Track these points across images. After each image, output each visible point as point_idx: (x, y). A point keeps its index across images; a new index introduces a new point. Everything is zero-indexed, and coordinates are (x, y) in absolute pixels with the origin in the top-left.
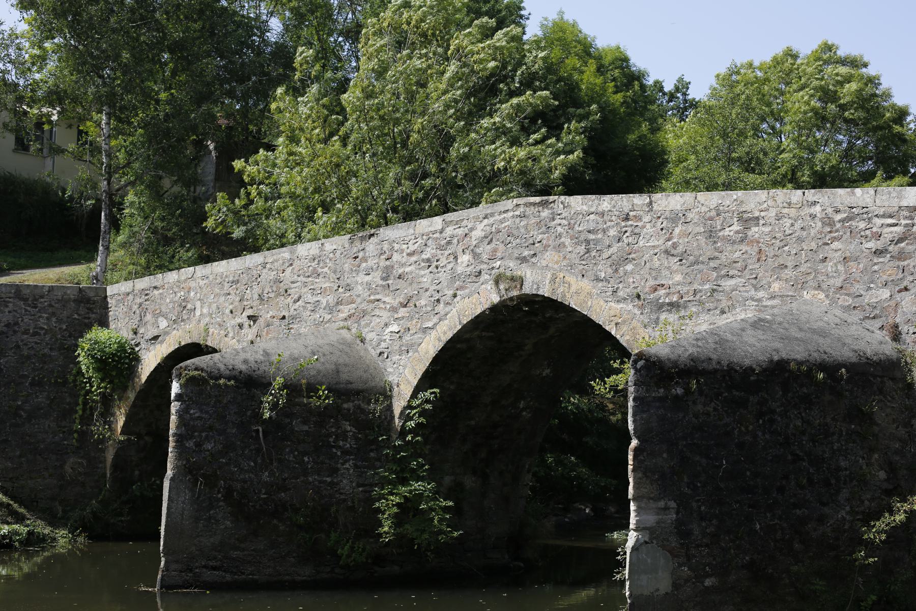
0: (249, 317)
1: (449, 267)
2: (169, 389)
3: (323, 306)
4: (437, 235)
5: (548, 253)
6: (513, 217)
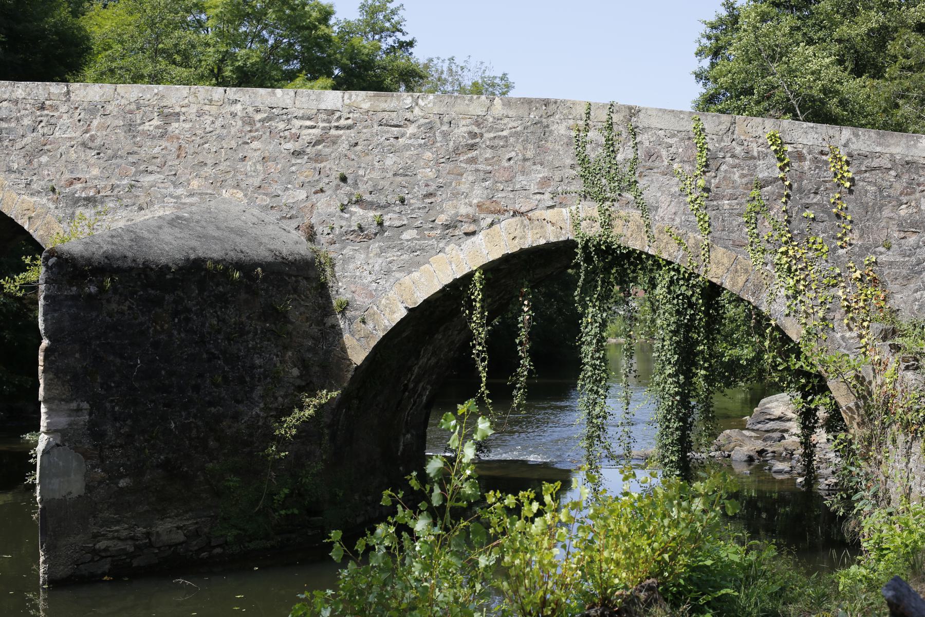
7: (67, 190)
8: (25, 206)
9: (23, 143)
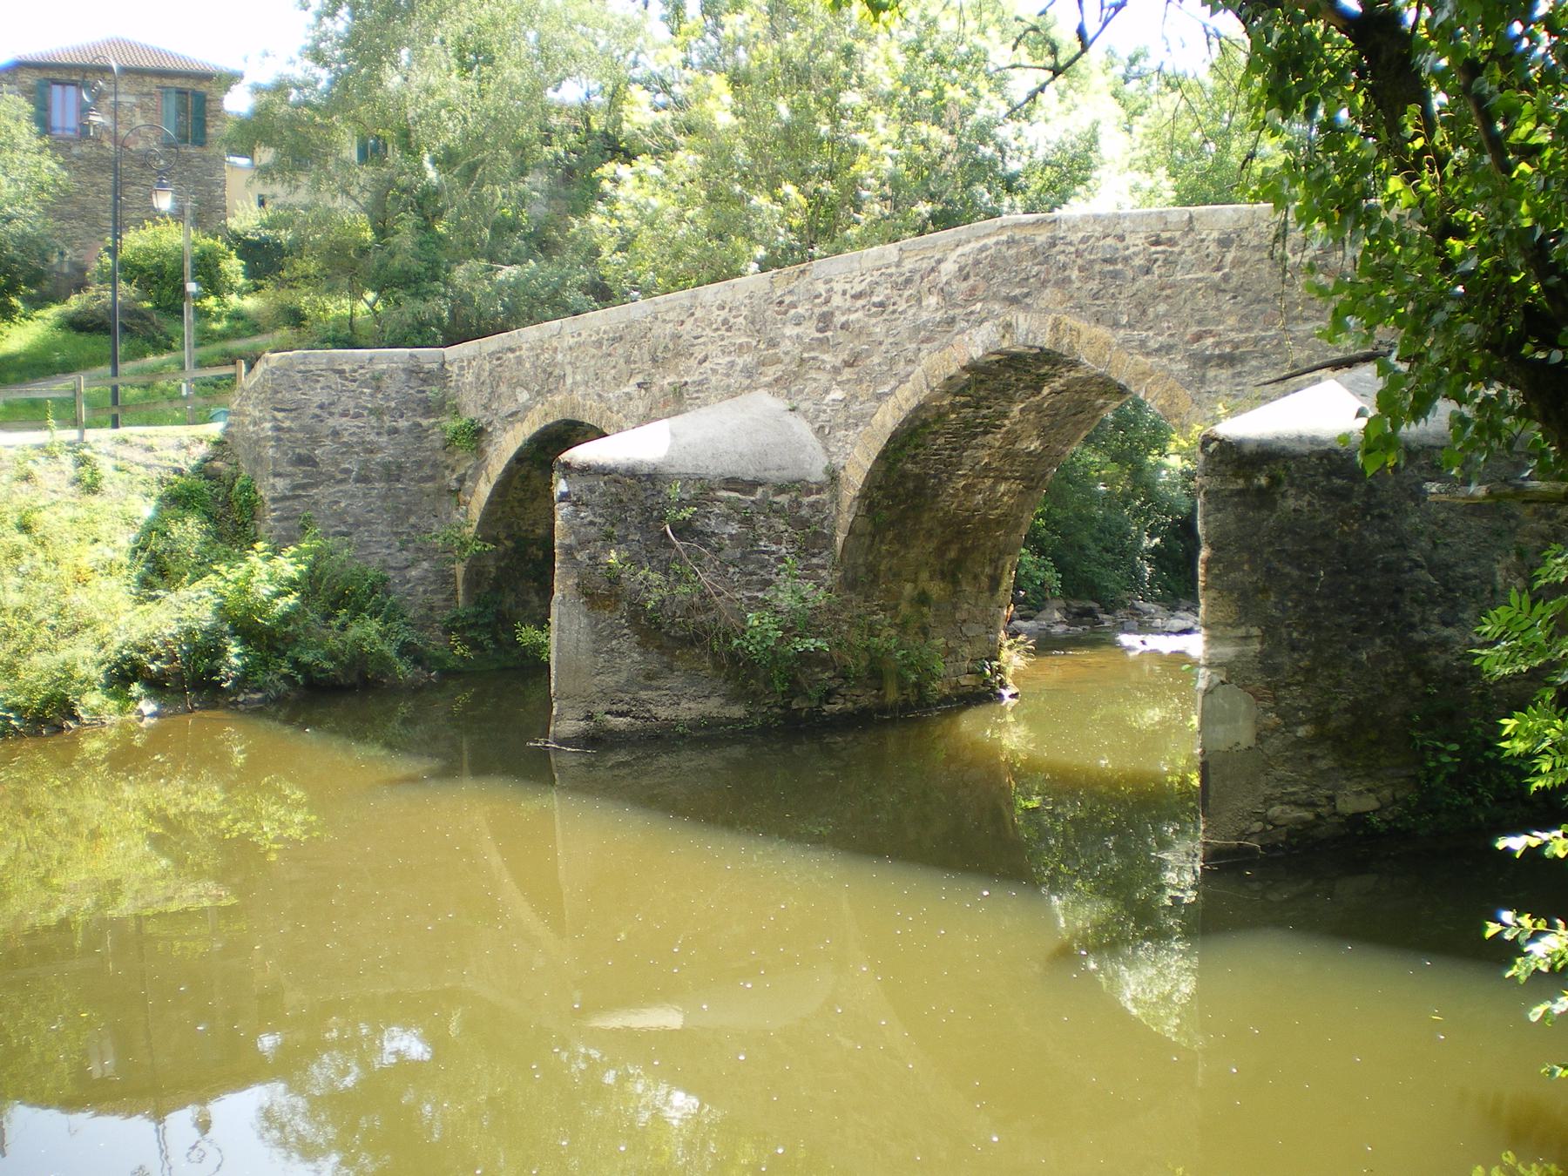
0: (639, 385)
1: (911, 312)
2: (1197, 554)
3: (738, 368)
4: (893, 270)
5: (1047, 291)
6: (997, 243)
7: (1195, 346)
8: (1140, 369)
9: (1134, 288)
